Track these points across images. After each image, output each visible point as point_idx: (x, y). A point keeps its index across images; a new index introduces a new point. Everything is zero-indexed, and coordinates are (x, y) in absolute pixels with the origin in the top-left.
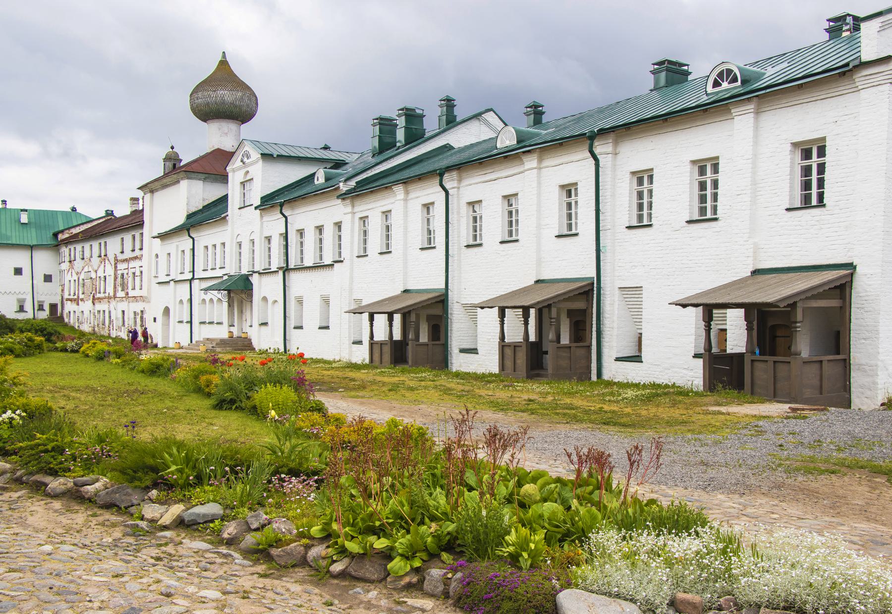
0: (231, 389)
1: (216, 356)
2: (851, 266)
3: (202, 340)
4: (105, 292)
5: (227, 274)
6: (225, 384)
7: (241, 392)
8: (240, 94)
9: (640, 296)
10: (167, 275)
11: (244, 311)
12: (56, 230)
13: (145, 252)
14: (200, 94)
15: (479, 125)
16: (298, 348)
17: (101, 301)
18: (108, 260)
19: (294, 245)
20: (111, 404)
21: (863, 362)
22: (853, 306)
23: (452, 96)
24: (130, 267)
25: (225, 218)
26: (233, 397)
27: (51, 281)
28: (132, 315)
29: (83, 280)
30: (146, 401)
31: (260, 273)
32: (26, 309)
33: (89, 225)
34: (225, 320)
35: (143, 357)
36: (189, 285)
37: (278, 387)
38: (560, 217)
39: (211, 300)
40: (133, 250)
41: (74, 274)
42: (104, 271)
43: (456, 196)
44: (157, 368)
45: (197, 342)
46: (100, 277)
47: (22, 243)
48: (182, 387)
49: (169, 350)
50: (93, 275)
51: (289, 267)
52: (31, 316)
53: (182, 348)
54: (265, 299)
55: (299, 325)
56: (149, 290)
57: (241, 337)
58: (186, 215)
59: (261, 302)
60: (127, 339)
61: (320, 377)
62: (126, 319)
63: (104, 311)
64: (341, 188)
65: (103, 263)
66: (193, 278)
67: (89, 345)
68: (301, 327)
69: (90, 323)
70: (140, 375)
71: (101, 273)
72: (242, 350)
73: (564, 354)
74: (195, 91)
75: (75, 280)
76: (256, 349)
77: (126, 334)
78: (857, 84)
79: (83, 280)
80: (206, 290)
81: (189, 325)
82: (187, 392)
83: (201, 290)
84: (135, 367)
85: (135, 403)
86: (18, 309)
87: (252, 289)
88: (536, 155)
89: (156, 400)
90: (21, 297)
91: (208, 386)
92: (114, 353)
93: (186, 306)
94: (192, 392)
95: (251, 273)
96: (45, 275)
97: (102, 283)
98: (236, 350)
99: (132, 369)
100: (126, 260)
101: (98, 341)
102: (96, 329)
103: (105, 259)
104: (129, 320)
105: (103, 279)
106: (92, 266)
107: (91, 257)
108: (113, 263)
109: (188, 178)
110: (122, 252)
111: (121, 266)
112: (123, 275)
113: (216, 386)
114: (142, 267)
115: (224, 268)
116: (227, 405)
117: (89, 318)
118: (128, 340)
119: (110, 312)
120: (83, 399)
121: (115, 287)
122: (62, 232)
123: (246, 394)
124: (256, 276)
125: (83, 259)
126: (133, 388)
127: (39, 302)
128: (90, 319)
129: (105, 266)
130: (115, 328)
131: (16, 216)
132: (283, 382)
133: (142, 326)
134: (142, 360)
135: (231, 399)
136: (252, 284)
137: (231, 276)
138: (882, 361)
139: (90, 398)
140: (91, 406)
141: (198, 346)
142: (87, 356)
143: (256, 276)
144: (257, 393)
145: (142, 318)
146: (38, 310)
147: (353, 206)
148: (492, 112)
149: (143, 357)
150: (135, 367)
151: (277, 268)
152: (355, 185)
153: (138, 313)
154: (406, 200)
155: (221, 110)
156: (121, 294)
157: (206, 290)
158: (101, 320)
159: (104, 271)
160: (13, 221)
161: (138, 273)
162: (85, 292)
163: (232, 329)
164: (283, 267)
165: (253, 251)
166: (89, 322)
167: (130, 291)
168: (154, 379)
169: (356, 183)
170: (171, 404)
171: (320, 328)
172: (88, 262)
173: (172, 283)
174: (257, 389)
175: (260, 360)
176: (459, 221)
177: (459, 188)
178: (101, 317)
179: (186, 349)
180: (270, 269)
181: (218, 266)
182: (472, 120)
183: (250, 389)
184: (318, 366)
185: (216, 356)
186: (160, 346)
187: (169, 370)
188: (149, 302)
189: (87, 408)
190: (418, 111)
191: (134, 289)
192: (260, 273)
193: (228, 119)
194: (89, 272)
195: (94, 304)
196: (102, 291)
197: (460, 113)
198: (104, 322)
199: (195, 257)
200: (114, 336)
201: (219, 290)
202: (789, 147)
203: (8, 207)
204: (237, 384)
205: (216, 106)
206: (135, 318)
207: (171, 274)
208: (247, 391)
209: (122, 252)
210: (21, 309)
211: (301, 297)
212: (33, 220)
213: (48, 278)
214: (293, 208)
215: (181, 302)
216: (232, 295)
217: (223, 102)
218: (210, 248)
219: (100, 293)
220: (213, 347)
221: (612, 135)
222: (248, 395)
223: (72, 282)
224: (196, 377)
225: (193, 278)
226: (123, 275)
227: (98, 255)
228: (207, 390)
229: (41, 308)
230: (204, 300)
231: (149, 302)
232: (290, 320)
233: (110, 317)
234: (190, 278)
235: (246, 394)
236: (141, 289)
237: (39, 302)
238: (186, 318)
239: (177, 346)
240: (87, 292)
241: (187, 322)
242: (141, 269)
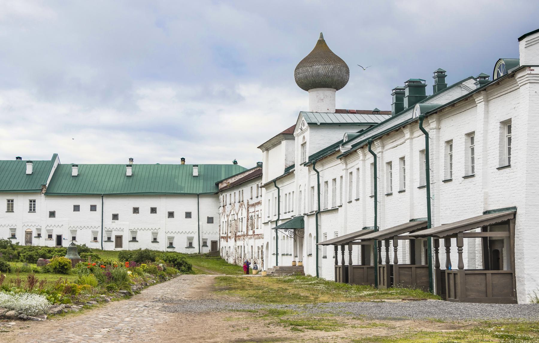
2: (515, 208)
8: (332, 67)
12: (219, 180)
14: (300, 70)
15: (461, 91)
19: (323, 194)
21: (519, 275)
22: (515, 236)
23: (444, 69)
24: (256, 210)
25: (293, 172)
27: (212, 222)
31: (308, 215)
32: (193, 245)
33: (242, 176)
38: (466, 160)
41: (226, 216)
43: (381, 158)
46: (239, 219)
47: (191, 192)
52: (197, 252)
58: (284, 169)
63: (241, 246)
64: (341, 150)
71: (240, 216)
73: (407, 273)
74: (297, 68)
75: (226, 222)
78: (519, 83)
83: (272, 229)
86: (188, 246)
87: (304, 228)
88: (408, 129)
90: (190, 235)
96: (208, 217)
100: (253, 205)
103: (242, 204)
105: (241, 220)
107: (235, 202)
108: (246, 208)
109: (286, 139)
110: (251, 199)
111: (251, 210)
121: (247, 227)
122: (221, 182)
127: (203, 239)
129: (242, 210)
131: (191, 171)
138: (528, 274)
146: (203, 246)
147: (346, 164)
148: (472, 79)
152: (351, 147)
154: (364, 160)
155: (317, 82)
156: (251, 232)
160: (188, 174)
167: (255, 230)
169: (352, 146)
173: (269, 222)
176: (383, 176)
177: (382, 152)
182: (454, 88)
190: (423, 82)
193: (323, 87)
195: (235, 241)
197: (449, 81)
202: (498, 125)
203: (186, 163)
205: (312, 78)
209: (251, 199)
210: (190, 245)
212: (202, 173)
213: (210, 220)
214: (323, 165)
217: (318, 75)
219: (239, 232)
221: (435, 116)
223: (225, 222)
225: (278, 220)
229: (205, 245)
234: (276, 220)
237: (203, 239)
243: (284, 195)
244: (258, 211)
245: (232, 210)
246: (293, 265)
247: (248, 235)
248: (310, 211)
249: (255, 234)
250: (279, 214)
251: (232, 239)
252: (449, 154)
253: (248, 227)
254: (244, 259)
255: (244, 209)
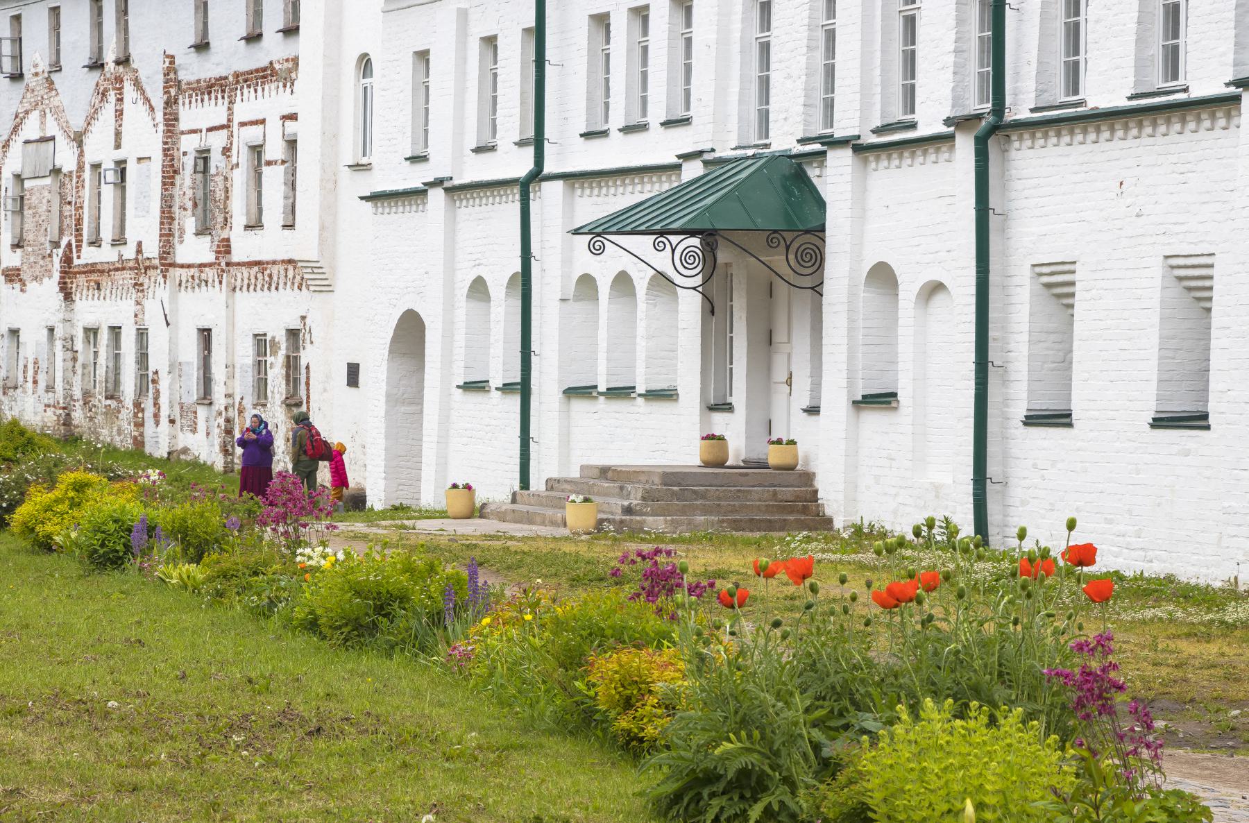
0: (744, 722)
1: (661, 559)
3: (575, 473)
4: (119, 241)
5: (698, 154)
6: (713, 699)
7: (793, 739)
9: (1207, 283)
10: (357, 167)
11: (780, 336)
13: (308, 44)
16: (1071, 525)
17: (105, 282)
18: (137, 83)
20: (173, 782)
26: (754, 758)
28: (246, 354)
29: (19, 178)
30: (334, 768)
31: (859, 149)
34: (689, 381)
35: (311, 555)
36: (516, 207)
37: (977, 721)
39: (623, 281)
40: (253, 38)
42: (118, 135)
44: (379, 609)
45: (551, 484)
46: (96, 166)
48: (501, 703)
49: (423, 525)
50: (66, 158)
51: (1009, 117)
53: (478, 512)
54: (883, 276)
55: (1055, 405)
56: (326, 231)
57: (763, 465)
59: (862, 293)
60: (219, 465)
61: (1164, 671)
62: (218, 372)
63: (115, 331)
65: (112, 97)
66: (537, 175)
67: (57, 493)
68: (1062, 419)
69: (50, 388)
70: (303, 641)
71: (99, 148)
72: (770, 526)
76: (838, 524)
77: (217, 442)
79: (19, 178)
80: (599, 232)
81: (515, 401)
82: (526, 731)
83: (577, 232)
84: (272, 603)
85: (283, 777)
89: (381, 767)
91: (628, 704)
92: (173, 533)
93: (504, 308)
94: (552, 733)
95: (817, 147)
97: (108, 193)
98: (737, 525)
99: (264, 612)
101: (92, 476)
102: (78, 416)
104: (231, 376)
105: (111, 176)
106: (57, 112)
107: (56, 67)
108: (158, 100)
110: (202, 46)
111: (195, 115)
112: (203, 156)
113: (669, 706)
114: (293, 117)
115: (686, 121)
116: (723, 801)
117: (43, 365)
118: (228, 469)
119: (142, 334)
120: (39, 757)
121: (167, 216)
123: (817, 747)
124: (840, 160)
125: (17, 77)
126: (272, 705)
128: (50, 372)
129: (119, 114)
130: (164, 412)
132: (1000, 692)
133: (292, 402)
134: (305, 570)
135: (744, 773)
136: (822, 204)
137: (721, 162)
139: (75, 752)
140: (80, 789)
141: (559, 503)
142: (46, 546)
143: (840, 160)
144: (873, 744)
145: (292, 364)
149: (311, 555)
150: (272, 603)
151: (948, 122)
153: (274, 344)
156: (193, 249)
157: (599, 232)
158: (101, 371)
159: (118, 135)
161: (274, 150)
162: (30, 237)
163: (720, 424)
164: (978, 117)
165: (831, 36)
166: (42, 385)
168: (368, 661)
170: (452, 789)
171: (1159, 423)
172: (41, 91)
173: (437, 195)
174: (870, 724)
175: (882, 582)
178: (102, 360)
179: (502, 516)
180: (913, 126)
181: (657, 114)
183: (836, 724)
184: (1149, 613)
185: (661, 559)
186: (376, 500)
187: (437, 619)
188: (327, 289)
189: (59, 798)
191: (255, 225)
192: (859, 149)
194: (43, 140)
195: (68, 297)
196: (107, 234)
198: (117, 383)
199: (549, 70)
200: (162, 452)
201: (662, 233)
204: (770, 698)
206: (261, 367)
207: (432, 151)
208: (817, 734)
209: (202, 46)
211: (1068, 266)
215: (479, 288)
216: (722, 256)
218: (620, 24)
219: (95, 243)
220: (628, 510)
222: (826, 752)
224: (573, 660)
225: (537, 175)
226: (203, 156)
227: (85, 57)
228: (624, 723)
230: (587, 283)
231: (327, 289)
232: (1005, 382)
233: (143, 359)
235: (817, 747)
236: (289, 226)
238: (502, 368)
239: (458, 503)
240: (39, 238)
241: (507, 388)
242: (291, 126)
243: (581, 31)
244: (263, 122)
245: (27, 112)
246: (709, 457)
247: (173, 265)
248: (878, 123)
249: (236, 257)
250: (538, 142)
251: (32, 286)
252: (757, 39)
253: (173, 219)
254: (137, 405)
255: (135, 113)
